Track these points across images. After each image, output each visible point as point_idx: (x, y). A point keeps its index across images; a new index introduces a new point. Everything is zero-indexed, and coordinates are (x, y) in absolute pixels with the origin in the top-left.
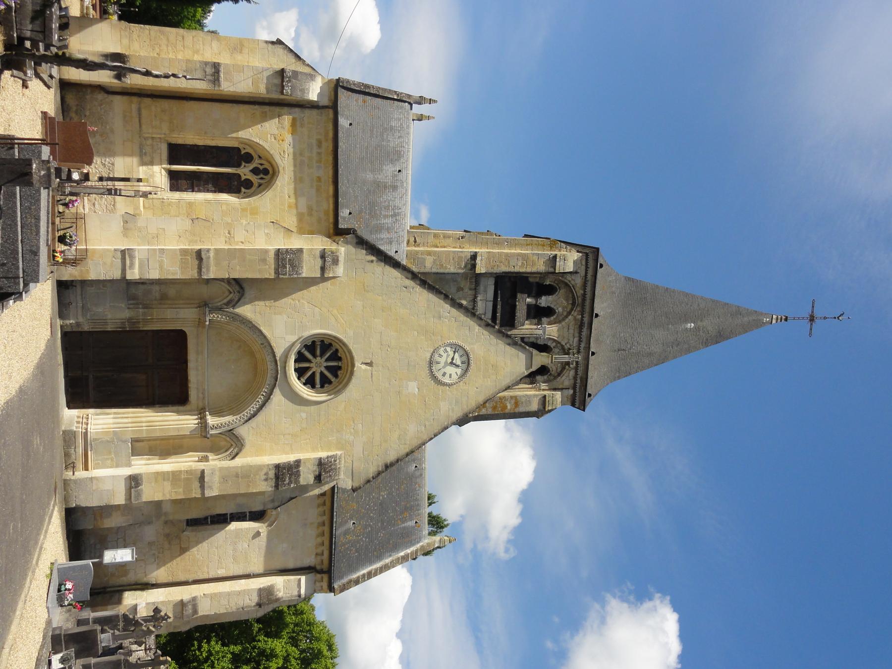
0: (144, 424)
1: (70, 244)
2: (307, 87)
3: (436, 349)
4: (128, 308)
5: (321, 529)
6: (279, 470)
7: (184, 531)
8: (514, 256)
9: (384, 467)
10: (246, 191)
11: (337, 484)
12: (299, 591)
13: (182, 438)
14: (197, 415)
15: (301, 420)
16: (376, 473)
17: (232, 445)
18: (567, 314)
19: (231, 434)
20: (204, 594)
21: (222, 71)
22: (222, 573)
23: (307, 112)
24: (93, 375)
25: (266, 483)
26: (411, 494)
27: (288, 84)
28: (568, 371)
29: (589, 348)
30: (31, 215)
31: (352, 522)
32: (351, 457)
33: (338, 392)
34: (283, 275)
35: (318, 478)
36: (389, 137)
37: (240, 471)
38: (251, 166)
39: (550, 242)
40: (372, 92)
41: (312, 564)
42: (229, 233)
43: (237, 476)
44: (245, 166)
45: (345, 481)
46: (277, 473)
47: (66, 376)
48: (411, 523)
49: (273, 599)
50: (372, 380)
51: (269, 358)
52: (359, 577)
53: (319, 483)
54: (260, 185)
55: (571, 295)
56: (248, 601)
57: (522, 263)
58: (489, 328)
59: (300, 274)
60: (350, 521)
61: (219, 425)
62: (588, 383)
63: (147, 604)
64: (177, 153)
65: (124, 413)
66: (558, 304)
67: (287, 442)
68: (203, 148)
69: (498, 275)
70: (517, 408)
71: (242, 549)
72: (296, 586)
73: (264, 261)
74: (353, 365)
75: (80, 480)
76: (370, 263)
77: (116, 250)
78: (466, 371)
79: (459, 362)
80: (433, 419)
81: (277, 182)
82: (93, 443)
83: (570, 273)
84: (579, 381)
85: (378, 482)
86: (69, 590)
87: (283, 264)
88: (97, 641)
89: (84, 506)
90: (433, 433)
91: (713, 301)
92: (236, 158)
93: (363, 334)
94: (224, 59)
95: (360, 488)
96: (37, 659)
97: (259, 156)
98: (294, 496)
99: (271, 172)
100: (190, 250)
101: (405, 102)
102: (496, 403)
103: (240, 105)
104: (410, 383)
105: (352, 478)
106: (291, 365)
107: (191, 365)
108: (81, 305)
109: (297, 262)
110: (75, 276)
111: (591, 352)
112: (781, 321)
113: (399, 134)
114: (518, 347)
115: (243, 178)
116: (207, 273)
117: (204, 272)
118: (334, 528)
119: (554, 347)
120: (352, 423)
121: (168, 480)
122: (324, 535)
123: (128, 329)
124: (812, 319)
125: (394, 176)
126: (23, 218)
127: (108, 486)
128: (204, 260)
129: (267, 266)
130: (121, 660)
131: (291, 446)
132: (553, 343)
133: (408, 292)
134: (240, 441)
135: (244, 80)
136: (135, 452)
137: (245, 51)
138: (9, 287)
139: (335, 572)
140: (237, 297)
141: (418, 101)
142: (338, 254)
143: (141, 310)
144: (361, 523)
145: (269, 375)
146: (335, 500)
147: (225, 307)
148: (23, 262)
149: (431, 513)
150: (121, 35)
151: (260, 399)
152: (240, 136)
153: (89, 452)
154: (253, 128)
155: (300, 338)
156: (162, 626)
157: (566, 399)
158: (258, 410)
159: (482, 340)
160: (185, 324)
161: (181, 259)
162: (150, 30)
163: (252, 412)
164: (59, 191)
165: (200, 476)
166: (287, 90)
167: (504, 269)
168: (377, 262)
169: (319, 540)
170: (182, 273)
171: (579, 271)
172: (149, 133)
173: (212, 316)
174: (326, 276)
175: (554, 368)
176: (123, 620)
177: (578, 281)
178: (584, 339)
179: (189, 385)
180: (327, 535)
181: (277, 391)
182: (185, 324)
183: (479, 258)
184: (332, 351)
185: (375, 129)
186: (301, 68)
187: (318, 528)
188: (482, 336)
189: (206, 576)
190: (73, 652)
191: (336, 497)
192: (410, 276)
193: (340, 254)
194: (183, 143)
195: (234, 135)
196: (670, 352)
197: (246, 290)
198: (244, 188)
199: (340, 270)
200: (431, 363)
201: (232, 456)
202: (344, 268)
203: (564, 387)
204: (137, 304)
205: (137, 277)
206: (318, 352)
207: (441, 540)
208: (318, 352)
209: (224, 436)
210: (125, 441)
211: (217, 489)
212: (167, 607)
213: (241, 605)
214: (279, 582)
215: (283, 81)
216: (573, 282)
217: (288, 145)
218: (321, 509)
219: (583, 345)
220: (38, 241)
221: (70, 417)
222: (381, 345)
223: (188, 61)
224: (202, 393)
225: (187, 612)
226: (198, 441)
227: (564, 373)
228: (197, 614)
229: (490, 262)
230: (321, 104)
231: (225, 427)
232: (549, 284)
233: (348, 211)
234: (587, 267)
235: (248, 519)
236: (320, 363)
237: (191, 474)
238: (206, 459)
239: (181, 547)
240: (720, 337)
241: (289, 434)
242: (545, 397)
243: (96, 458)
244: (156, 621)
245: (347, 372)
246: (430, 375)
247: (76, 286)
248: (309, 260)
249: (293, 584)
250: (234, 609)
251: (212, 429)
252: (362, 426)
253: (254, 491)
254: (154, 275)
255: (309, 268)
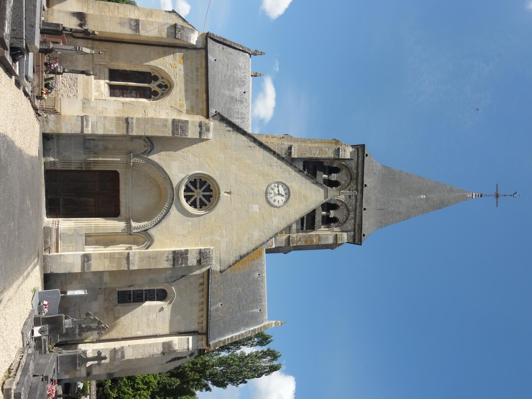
0: (93, 226)
1: (52, 88)
2: (190, 36)
3: (269, 185)
4: (85, 154)
5: (202, 287)
6: (175, 255)
7: (116, 306)
8: (314, 148)
9: (239, 258)
10: (155, 97)
11: (211, 268)
12: (188, 346)
13: (116, 235)
14: (126, 222)
15: (189, 226)
16: (235, 261)
17: (146, 240)
18: (348, 185)
19: (146, 233)
20: (128, 345)
21: (141, 24)
22: (139, 334)
23: (190, 52)
24: (63, 198)
25: (166, 263)
26: (256, 292)
27: (178, 32)
28: (350, 220)
29: (362, 205)
30: (31, 4)
31: (220, 304)
32: (219, 251)
33: (210, 210)
34: (177, 135)
35: (199, 262)
36: (238, 71)
37: (151, 254)
38: (158, 83)
39: (335, 141)
40: (227, 43)
41: (196, 330)
42: (145, 112)
43: (149, 257)
44: (154, 83)
45: (216, 267)
46: (174, 256)
47: (46, 198)
48: (257, 310)
49: (172, 351)
50: (231, 203)
51: (169, 186)
52: (225, 339)
53: (200, 265)
54: (163, 94)
55: (349, 174)
56: (156, 351)
57: (319, 152)
58: (301, 173)
59: (187, 136)
60: (219, 303)
61: (139, 227)
62: (363, 228)
63: (93, 350)
64: (114, 74)
65: (80, 220)
66: (342, 179)
67: (180, 240)
68: (129, 72)
69: (305, 160)
70: (320, 242)
71: (152, 319)
72: (186, 343)
73: (165, 126)
74: (219, 193)
75: (53, 256)
76: (228, 132)
77: (78, 116)
78: (288, 199)
79: (283, 193)
80: (269, 228)
81: (172, 91)
82: (61, 236)
83: (348, 159)
84: (357, 226)
85: (236, 280)
86: (45, 305)
87: (177, 128)
88: (62, 324)
89: (56, 273)
90: (269, 237)
91: (436, 182)
92: (149, 78)
93: (225, 174)
94: (142, 18)
95: (225, 270)
96: (25, 322)
97: (162, 77)
98: (185, 275)
99: (169, 86)
100: (122, 118)
101: (247, 52)
102: (307, 238)
103: (151, 46)
104: (254, 205)
105: (220, 264)
106: (182, 194)
107: (121, 192)
108: (57, 150)
109: (185, 128)
110: (54, 131)
111: (364, 185)
112: (478, 197)
113: (244, 71)
114: (318, 185)
115: (153, 90)
116: (132, 132)
117: (130, 131)
118: (209, 306)
119: (341, 205)
120: (219, 229)
121: (107, 258)
122: (203, 310)
123: (84, 169)
124: (497, 196)
125: (241, 95)
126: (27, 5)
127: (70, 261)
128: (130, 124)
129: (168, 129)
130: (77, 355)
131: (182, 243)
132: (340, 203)
133: (251, 150)
134: (151, 237)
135: (153, 30)
136: (87, 243)
137: (154, 16)
138: (17, 43)
139: (210, 335)
140: (149, 149)
141: (254, 53)
142: (209, 125)
143: (92, 155)
144: (226, 305)
145: (169, 197)
146: (210, 287)
147: (142, 155)
148: (26, 31)
149: (269, 349)
150: (82, 5)
151: (164, 211)
152: (151, 65)
153: (59, 241)
154: (158, 59)
155: (187, 176)
156: (103, 333)
157: (350, 238)
158: (162, 218)
159: (297, 180)
160: (119, 166)
161: (116, 123)
162: (99, 3)
163: (159, 220)
164: (46, 46)
165: (127, 256)
166: (178, 36)
167: (308, 155)
168: (232, 131)
169: (200, 314)
170: (117, 131)
171: (353, 158)
172: (98, 62)
173: (134, 160)
174: (202, 137)
175: (341, 219)
176: (78, 328)
177: (353, 164)
178: (359, 200)
179: (121, 204)
180: (205, 310)
181: (174, 207)
182: (119, 166)
183: (293, 149)
184: (206, 186)
185: (230, 66)
186: (185, 25)
187: (199, 306)
188: (297, 178)
189: (130, 336)
190: (47, 327)
191: (210, 285)
192: (252, 140)
193: (211, 126)
194: (118, 69)
195: (147, 64)
196: (412, 213)
197: (155, 145)
198: (154, 96)
199: (211, 135)
200: (266, 193)
201: (147, 247)
202: (213, 134)
203: (348, 230)
204: (90, 152)
205: (90, 133)
206: (198, 186)
207: (276, 322)
208: (198, 186)
209: (141, 235)
210: (81, 235)
211: (137, 265)
212: (105, 353)
213: (152, 353)
214: (175, 340)
215: (176, 31)
216: (350, 165)
217: (179, 71)
218: (201, 294)
219: (358, 204)
220: (35, 19)
221: (48, 221)
222: (236, 181)
223: (121, 18)
224: (128, 209)
225: (118, 356)
226: (125, 238)
227: (347, 221)
228: (124, 358)
229: (300, 151)
230: (198, 47)
231: (142, 228)
232: (336, 167)
233: (215, 110)
234: (358, 156)
235: (156, 300)
236: (200, 192)
237: (122, 255)
238: (131, 248)
239: (114, 317)
240: (442, 205)
241: (181, 235)
242: (336, 235)
243: (63, 245)
244: (99, 330)
245: (216, 198)
246: (266, 201)
247: (54, 139)
248: (192, 128)
249: (184, 341)
250: (147, 356)
251: (134, 229)
252: (226, 231)
253: (160, 267)
254: (100, 132)
255: (192, 133)
